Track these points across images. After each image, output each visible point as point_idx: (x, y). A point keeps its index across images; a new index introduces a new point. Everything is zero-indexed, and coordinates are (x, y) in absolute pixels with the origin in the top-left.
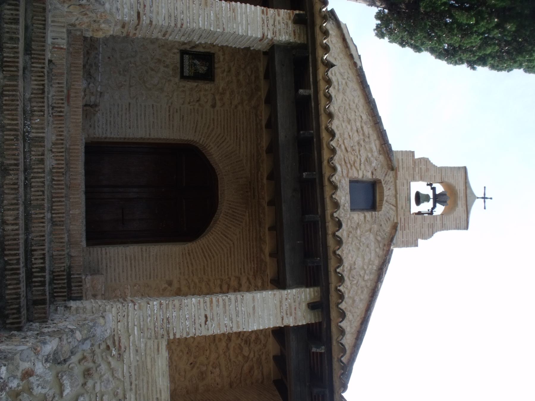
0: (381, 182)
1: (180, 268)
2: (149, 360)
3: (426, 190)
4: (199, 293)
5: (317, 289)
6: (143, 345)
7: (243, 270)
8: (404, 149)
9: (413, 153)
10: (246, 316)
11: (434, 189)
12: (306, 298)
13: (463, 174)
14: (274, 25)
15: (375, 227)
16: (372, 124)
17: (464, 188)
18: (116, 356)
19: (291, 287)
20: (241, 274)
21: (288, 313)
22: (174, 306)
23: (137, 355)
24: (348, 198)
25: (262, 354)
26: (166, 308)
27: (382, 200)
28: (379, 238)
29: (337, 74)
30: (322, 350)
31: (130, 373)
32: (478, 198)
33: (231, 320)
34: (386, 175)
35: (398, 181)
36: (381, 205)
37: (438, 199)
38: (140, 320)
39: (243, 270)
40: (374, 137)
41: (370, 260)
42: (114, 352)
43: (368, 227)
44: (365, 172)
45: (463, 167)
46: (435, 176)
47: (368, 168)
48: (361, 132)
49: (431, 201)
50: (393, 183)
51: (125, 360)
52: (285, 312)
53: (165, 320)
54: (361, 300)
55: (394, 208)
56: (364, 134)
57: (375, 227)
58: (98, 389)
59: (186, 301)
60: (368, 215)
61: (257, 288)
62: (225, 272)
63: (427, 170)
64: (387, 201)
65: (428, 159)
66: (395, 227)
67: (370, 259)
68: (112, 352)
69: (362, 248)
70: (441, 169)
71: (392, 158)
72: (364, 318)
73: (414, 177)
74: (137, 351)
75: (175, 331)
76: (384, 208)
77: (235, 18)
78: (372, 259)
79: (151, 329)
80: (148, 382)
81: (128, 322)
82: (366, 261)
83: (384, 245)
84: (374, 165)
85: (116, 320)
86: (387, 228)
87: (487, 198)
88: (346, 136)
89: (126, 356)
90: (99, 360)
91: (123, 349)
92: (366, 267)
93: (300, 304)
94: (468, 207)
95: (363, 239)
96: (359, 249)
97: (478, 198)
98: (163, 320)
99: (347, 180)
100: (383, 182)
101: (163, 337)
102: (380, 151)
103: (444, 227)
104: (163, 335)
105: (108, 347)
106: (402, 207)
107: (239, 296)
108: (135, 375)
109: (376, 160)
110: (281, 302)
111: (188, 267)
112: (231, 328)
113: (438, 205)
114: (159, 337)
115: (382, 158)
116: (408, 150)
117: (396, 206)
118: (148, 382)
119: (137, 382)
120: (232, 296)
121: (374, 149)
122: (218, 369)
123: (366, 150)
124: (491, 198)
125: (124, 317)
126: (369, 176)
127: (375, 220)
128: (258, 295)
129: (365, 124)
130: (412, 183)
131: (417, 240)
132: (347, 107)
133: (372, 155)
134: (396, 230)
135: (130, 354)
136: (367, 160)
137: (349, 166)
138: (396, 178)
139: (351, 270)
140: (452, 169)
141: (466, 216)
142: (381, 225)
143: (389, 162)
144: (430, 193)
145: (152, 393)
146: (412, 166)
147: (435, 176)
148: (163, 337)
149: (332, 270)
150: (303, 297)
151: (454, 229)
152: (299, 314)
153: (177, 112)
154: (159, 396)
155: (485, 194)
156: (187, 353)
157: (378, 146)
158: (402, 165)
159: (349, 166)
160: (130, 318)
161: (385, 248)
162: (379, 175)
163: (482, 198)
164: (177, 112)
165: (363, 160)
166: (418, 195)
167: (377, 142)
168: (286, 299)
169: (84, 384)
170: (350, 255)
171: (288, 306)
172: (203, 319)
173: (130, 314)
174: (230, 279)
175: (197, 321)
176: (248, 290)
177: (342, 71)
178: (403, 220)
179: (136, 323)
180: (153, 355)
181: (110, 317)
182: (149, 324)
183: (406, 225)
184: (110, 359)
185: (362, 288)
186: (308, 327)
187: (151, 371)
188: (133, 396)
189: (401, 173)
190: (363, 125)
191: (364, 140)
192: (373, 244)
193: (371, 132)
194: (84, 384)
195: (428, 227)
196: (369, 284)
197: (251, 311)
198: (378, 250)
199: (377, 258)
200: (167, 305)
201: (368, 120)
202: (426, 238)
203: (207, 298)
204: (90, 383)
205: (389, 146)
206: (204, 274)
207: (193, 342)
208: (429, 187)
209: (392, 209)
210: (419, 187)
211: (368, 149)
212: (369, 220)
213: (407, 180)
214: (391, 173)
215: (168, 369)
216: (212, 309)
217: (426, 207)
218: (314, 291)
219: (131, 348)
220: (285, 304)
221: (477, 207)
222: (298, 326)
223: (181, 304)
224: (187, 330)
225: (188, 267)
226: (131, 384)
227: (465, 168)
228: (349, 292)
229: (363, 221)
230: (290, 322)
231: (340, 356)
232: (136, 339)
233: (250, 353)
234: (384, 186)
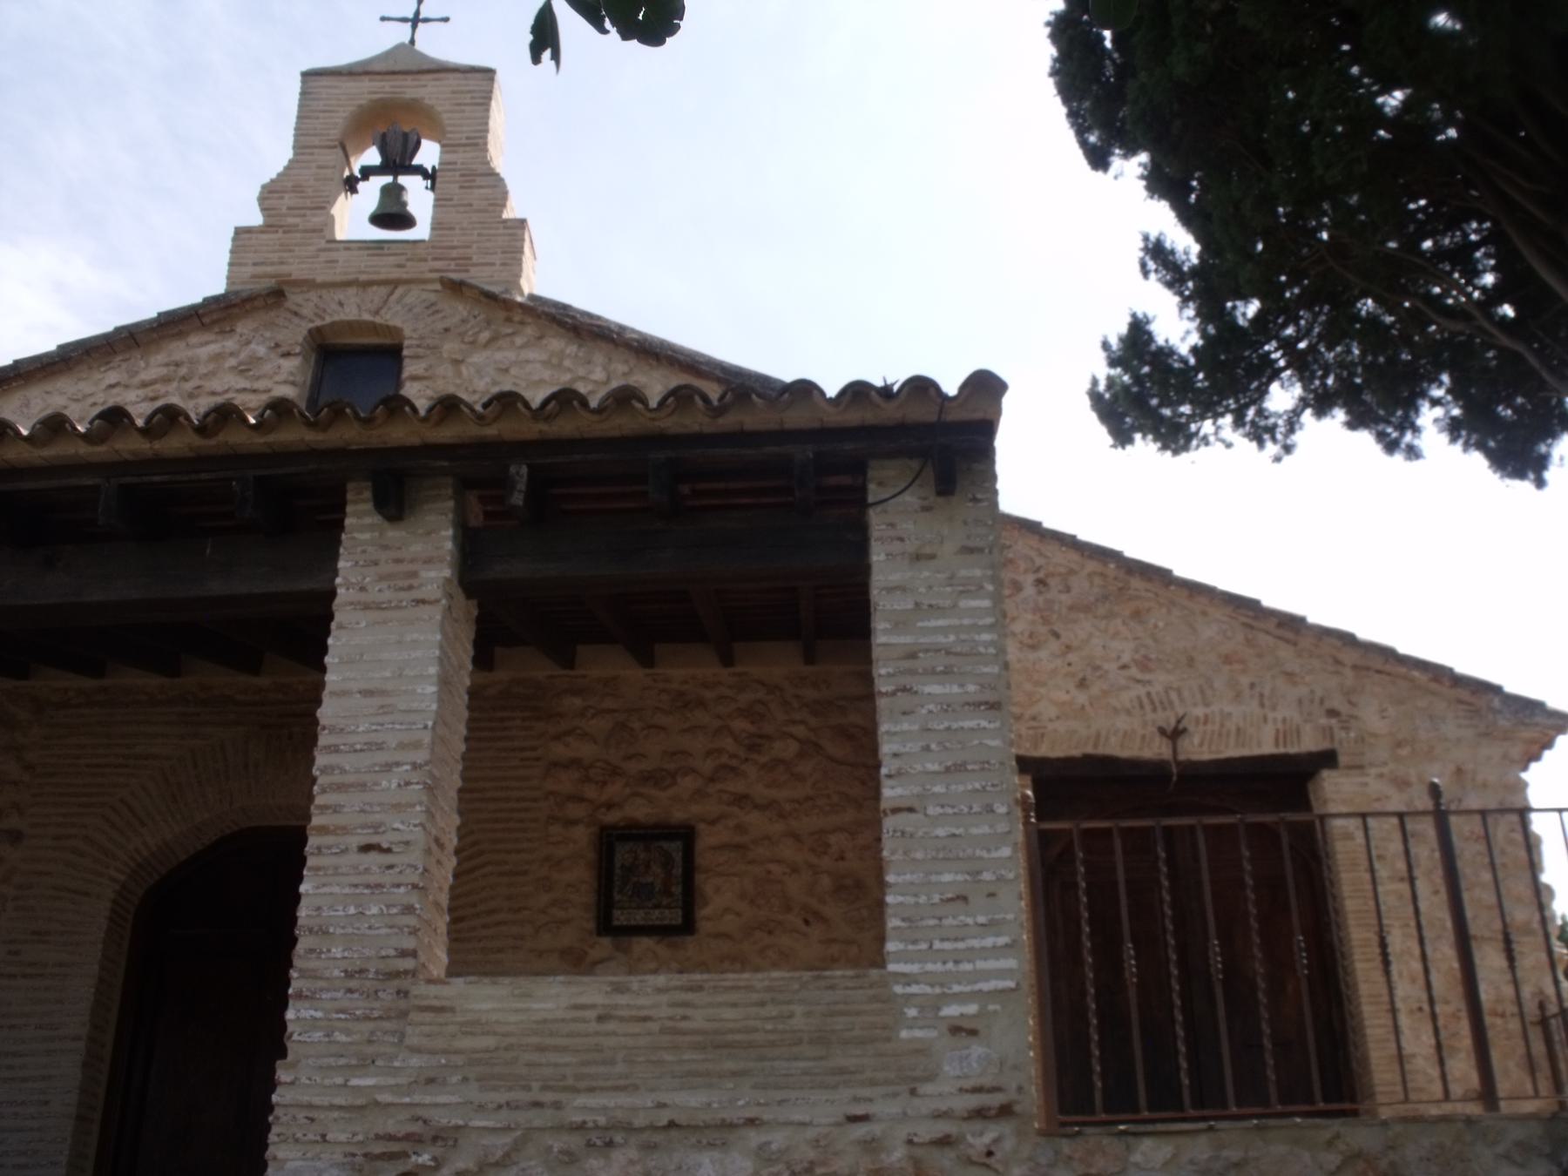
0: (319, 330)
1: (500, 951)
2: (466, 1043)
3: (370, 193)
6: (415, 1061)
7: (528, 754)
8: (225, 258)
9: (240, 232)
10: (387, 718)
11: (367, 172)
12: (371, 528)
13: (325, 81)
15: (450, 347)
16: (137, 354)
17: (367, 78)
18: (437, 1150)
20: (538, 759)
21: (406, 583)
22: (312, 951)
23: (444, 1083)
25: (797, 696)
26: (316, 978)
27: (374, 328)
28: (485, 336)
30: (520, 472)
31: (500, 1107)
33: (388, 767)
34: (296, 314)
35: (319, 279)
37: (398, 161)
38: (330, 1068)
39: (528, 754)
40: (178, 350)
42: (425, 1158)
43: (445, 370)
44: (277, 378)
45: (304, 82)
46: (320, 167)
47: (267, 368)
48: (157, 386)
49: (403, 180)
50: (324, 292)
51: (453, 1122)
52: (402, 595)
53: (353, 984)
55: (400, 291)
56: (166, 380)
62: (526, 810)
63: (298, 189)
64: (377, 313)
65: (264, 187)
66: (456, 288)
67: (543, 363)
68: (424, 1167)
70: (299, 147)
71: (244, 295)
73: (314, 231)
74: (431, 1081)
75: (392, 952)
78: (544, 357)
79: (372, 1033)
80: (541, 1049)
81: (332, 1107)
83: (509, 320)
84: (261, 350)
85: (318, 1148)
86: (458, 310)
87: (417, 13)
89: (443, 1119)
91: (416, 1128)
93: (386, 547)
94: (425, 67)
98: (350, 991)
100: (318, 323)
101: (406, 994)
102: (222, 332)
103: (477, 141)
104: (398, 993)
106: (400, 266)
108: (510, 1089)
109: (248, 343)
110: (366, 607)
111: (498, 924)
112: (415, 766)
113: (416, 161)
114: (402, 1004)
115: (244, 327)
116: (228, 245)
117: (395, 283)
118: (541, 1049)
119: (535, 1085)
121: (214, 348)
122: (833, 839)
123: (213, 374)
125: (312, 1120)
127: (428, 347)
130: (340, 235)
131: (506, 221)
133: (232, 354)
135: (436, 1105)
136: (242, 371)
138: (308, 285)
140: (304, 114)
141: (451, 76)
142: (447, 330)
143: (256, 303)
145: (579, 1035)
146: (280, 235)
147: (320, 167)
148: (406, 994)
149: (262, 440)
150: (367, 536)
151: (488, 110)
152: (417, 548)
153: (17, 953)
154: (591, 1014)
156: (770, 932)
158: (272, 264)
160: (317, 1101)
161: (517, 318)
162: (295, 334)
163: (414, 27)
164: (17, 953)
165: (247, 385)
166: (379, 219)
167: (194, 339)
168: (363, 589)
171: (384, 585)
172: (373, 858)
173: (305, 1099)
174: (552, 793)
175: (372, 879)
178: (438, 264)
179: (339, 1080)
180: (452, 1029)
182: (356, 1037)
183: (454, 254)
187: (504, 1035)
188: (581, 1100)
190: (136, 381)
192: (499, 356)
193: (161, 358)
195: (474, 187)
197: (376, 701)
198: (519, 341)
199: (544, 342)
201: (124, 365)
202: (504, 195)
205: (211, 302)
206: (525, 873)
207: (738, 914)
208: (361, 186)
209: (402, 297)
211: (211, 367)
212: (423, 365)
213: (320, 250)
214: (294, 298)
215: (507, 980)
216: (344, 828)
217: (419, 197)
218: (355, 502)
219: (417, 1098)
220: (380, 593)
221: (435, 45)
223: (311, 931)
224: (394, 911)
225: (498, 924)
226: (537, 1104)
227: (308, 76)
229: (425, 383)
231: (523, 410)
232: (391, 1081)
233: (792, 736)
234: (328, 320)
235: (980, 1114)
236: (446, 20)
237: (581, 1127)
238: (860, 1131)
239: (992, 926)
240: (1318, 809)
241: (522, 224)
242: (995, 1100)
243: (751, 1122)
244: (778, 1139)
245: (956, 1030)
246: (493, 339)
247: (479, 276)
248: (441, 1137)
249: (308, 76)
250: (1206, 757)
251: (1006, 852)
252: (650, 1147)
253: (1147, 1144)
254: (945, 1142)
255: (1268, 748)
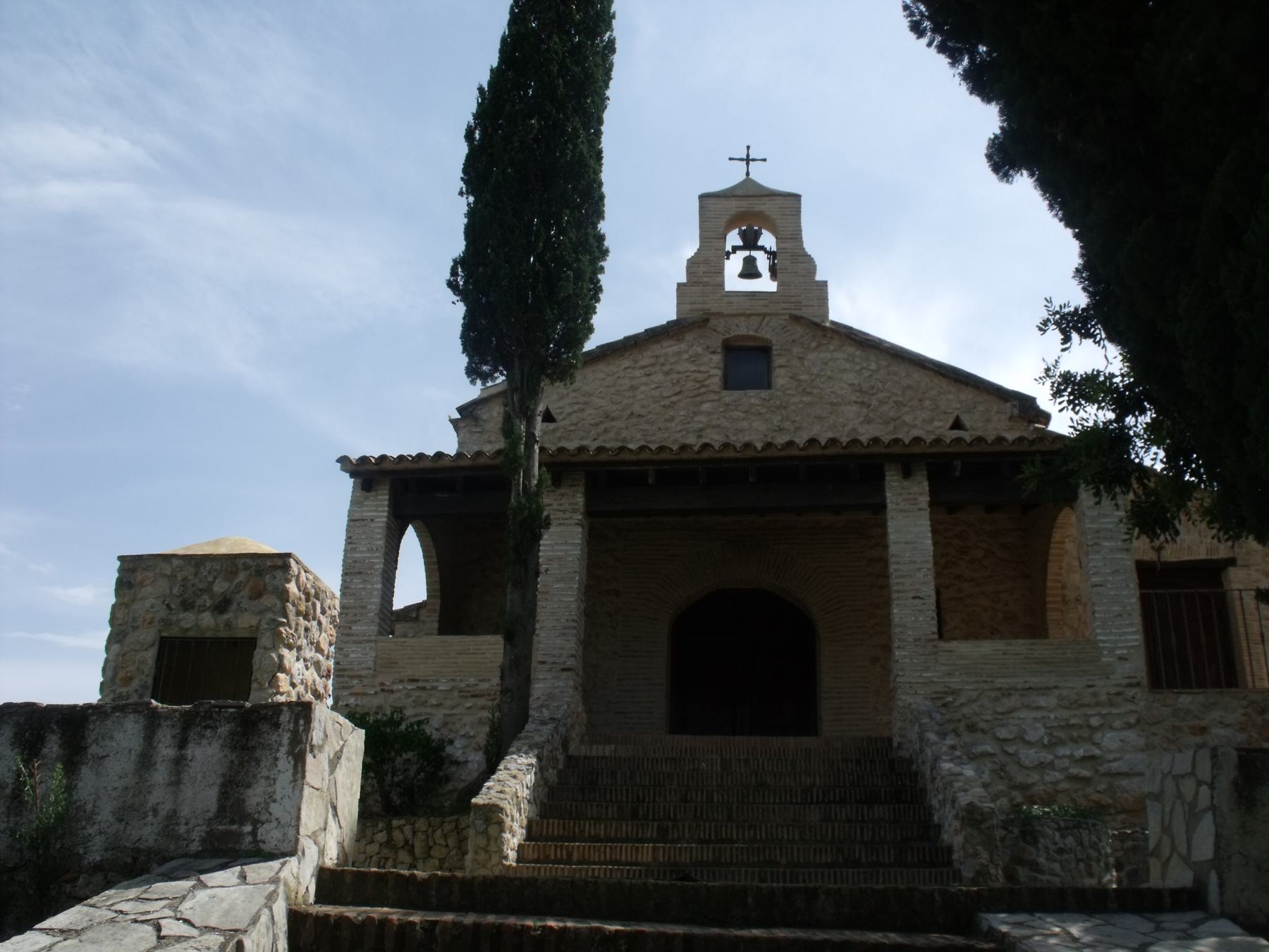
4: (888, 603)
5: (886, 468)
6: (943, 668)
9: (679, 285)
11: (735, 249)
13: (712, 201)
14: (564, 511)
15: (796, 350)
19: (884, 498)
24: (752, 393)
27: (754, 338)
28: (814, 344)
29: (561, 404)
30: (958, 464)
32: (748, 174)
33: (919, 569)
36: (763, 339)
37: (750, 242)
40: (656, 349)
41: (847, 360)
42: (950, 699)
43: (795, 362)
47: (706, 359)
49: (755, 253)
54: (908, 375)
55: (767, 319)
56: (653, 365)
57: (796, 350)
58: (989, 717)
59: (896, 620)
60: (778, 361)
61: (884, 535)
66: (797, 319)
69: (829, 373)
70: (703, 238)
72: (935, 371)
76: (768, 336)
77: (560, 558)
82: (848, 366)
83: (824, 336)
84: (700, 350)
86: (799, 330)
88: (656, 393)
89: (954, 686)
90: (958, 715)
92: (858, 368)
95: (815, 371)
96: (829, 378)
97: (748, 174)
99: (725, 393)
103: (797, 236)
105: (945, 705)
107: (892, 560)
110: (901, 511)
113: (760, 243)
115: (689, 337)
117: (764, 315)
120: (892, 568)
121: (675, 348)
123: (677, 362)
124: (748, 148)
126: (717, 358)
128: (892, 537)
129: (636, 362)
132: (612, 390)
134: (802, 317)
136: (694, 359)
137: (703, 390)
138: (720, 315)
139: (861, 391)
144: (742, 254)
155: (742, 160)
157: (671, 342)
159: (703, 390)
162: (717, 342)
165: (693, 368)
166: (744, 275)
167: (665, 344)
169: (983, 731)
170: (839, 392)
172: (917, 601)
176: (886, 547)
177: (555, 397)
178: (784, 305)
181: (910, 700)
183: (793, 299)
184: (957, 703)
185: (889, 374)
186: (931, 479)
189: (713, 307)
190: (639, 365)
191: (663, 365)
192: (822, 355)
193: (649, 353)
194: (983, 731)
195: (794, 264)
196: (884, 363)
198: (831, 347)
200: (900, 640)
202: (814, 267)
203: (895, 596)
204: (982, 725)
210: (733, 281)
214: (713, 322)
222: (930, 491)
227: (704, 198)
228: (896, 394)
230: (924, 500)
235: (1130, 685)
236: (765, 160)
237: (1000, 689)
238: (1091, 690)
239: (1131, 625)
240: (1226, 588)
241: (825, 284)
242: (1134, 681)
243: (1056, 687)
244: (1065, 692)
245: (1121, 658)
246: (818, 346)
247: (806, 312)
248: (955, 692)
249: (704, 198)
250: (1174, 560)
251: (1134, 600)
252: (1022, 695)
253: (1184, 696)
254: (1118, 694)
255: (1203, 556)
